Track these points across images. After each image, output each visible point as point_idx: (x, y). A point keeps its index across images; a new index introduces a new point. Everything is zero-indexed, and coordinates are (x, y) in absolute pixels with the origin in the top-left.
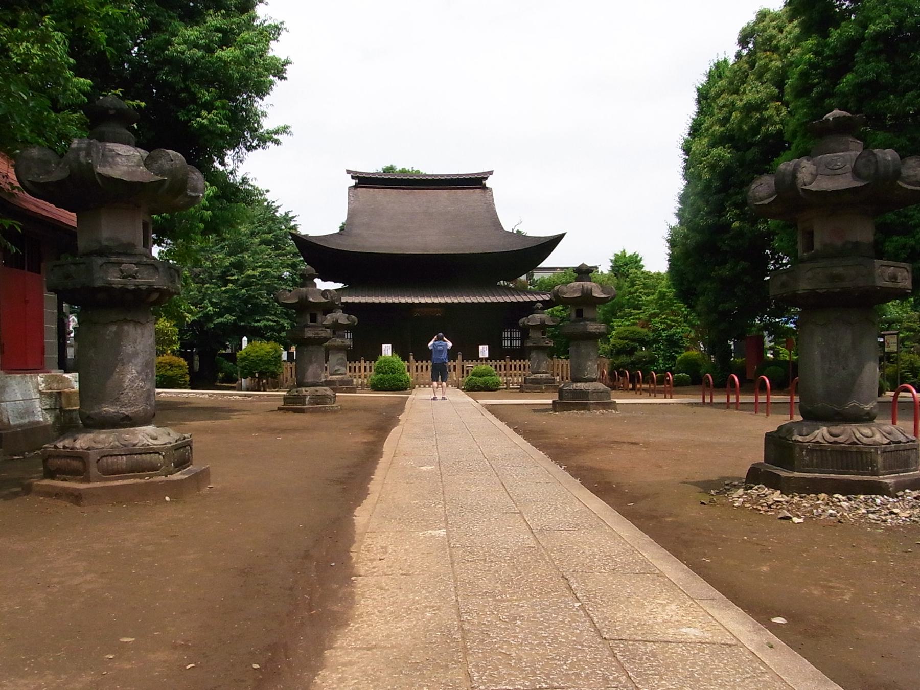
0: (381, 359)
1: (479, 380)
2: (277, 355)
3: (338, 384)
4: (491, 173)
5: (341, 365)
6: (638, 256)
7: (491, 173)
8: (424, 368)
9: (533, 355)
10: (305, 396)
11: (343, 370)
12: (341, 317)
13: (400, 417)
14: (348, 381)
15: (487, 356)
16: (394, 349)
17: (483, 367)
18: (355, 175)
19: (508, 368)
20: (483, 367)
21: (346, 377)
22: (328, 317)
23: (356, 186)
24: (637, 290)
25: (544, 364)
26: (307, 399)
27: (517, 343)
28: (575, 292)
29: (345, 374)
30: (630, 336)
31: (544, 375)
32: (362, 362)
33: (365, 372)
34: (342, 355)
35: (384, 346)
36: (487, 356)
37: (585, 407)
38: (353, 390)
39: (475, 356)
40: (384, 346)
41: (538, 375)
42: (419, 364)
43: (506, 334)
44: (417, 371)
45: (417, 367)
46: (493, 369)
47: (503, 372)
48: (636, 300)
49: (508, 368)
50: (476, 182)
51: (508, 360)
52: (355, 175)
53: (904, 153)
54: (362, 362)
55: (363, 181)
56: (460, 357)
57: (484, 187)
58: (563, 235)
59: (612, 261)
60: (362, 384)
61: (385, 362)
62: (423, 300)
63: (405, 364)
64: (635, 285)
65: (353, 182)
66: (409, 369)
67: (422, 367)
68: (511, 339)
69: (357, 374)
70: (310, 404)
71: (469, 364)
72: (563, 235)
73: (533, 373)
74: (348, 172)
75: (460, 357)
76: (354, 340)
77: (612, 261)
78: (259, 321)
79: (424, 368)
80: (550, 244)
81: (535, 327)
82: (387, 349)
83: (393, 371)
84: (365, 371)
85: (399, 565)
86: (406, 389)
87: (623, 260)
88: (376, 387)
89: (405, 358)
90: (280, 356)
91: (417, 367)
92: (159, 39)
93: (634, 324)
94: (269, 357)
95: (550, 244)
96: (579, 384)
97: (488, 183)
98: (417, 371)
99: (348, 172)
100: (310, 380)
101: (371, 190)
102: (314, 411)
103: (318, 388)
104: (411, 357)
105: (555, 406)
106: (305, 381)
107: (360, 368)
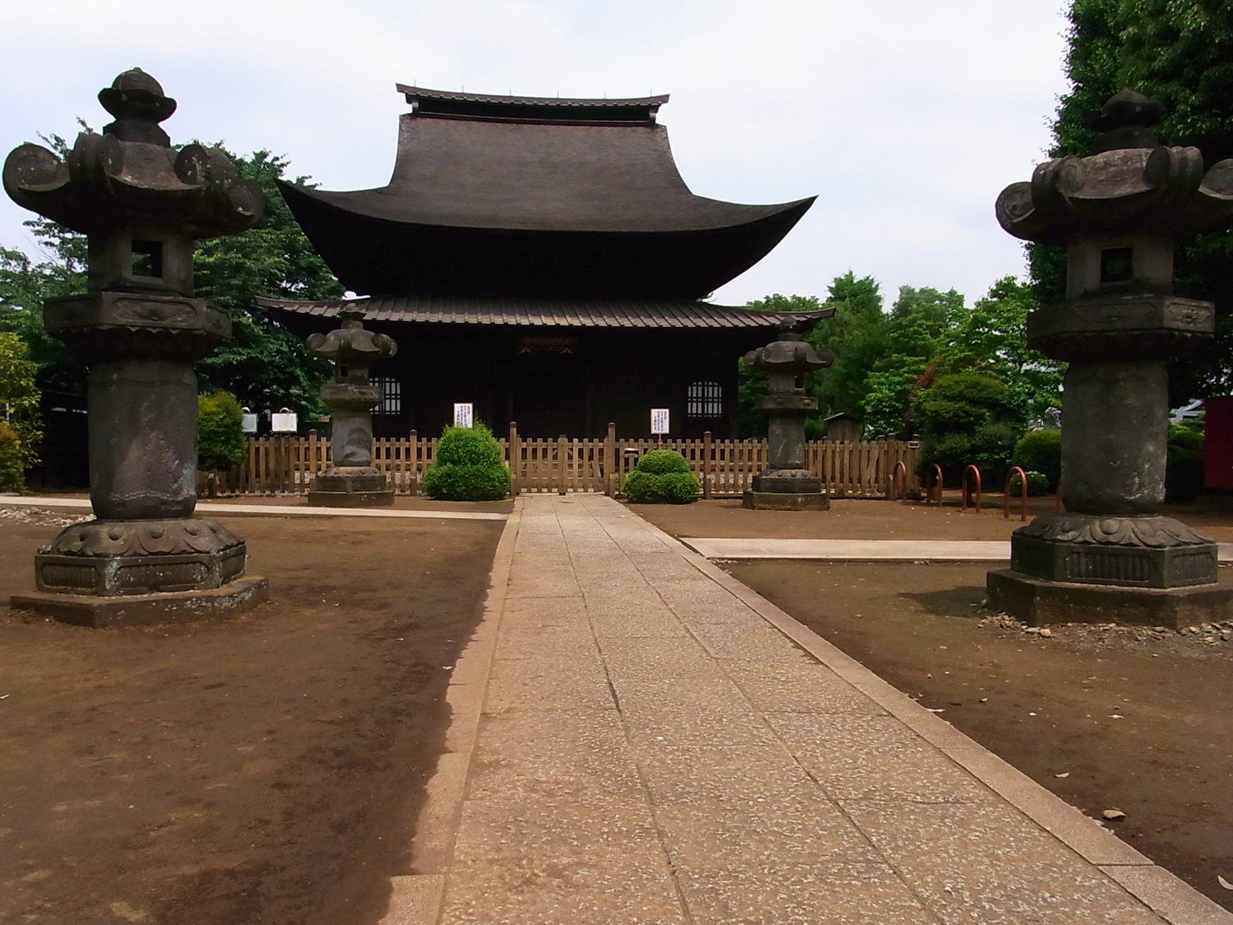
0: (449, 432)
1: (657, 480)
2: (228, 421)
3: (349, 484)
4: (665, 99)
5: (357, 443)
6: (872, 281)
7: (665, 99)
8: (540, 453)
9: (776, 428)
10: (102, 559)
11: (362, 455)
12: (363, 341)
13: (486, 604)
14: (373, 479)
15: (666, 430)
16: (478, 414)
17: (664, 453)
18: (412, 95)
19: (708, 454)
20: (664, 453)
21: (369, 471)
22: (331, 336)
23: (414, 115)
24: (914, 321)
25: (798, 450)
26: (112, 568)
27: (714, 409)
28: (1117, 179)
29: (368, 464)
30: (972, 393)
31: (799, 473)
32: (413, 439)
33: (414, 461)
34: (361, 423)
35: (457, 406)
36: (666, 430)
37: (1155, 611)
38: (383, 500)
39: (641, 430)
40: (457, 406)
41: (787, 473)
42: (529, 444)
43: (694, 391)
44: (524, 457)
45: (524, 450)
46: (679, 454)
47: (698, 462)
48: (911, 338)
49: (708, 454)
50: (638, 114)
51: (708, 440)
52: (412, 95)
53: (1212, 155)
54: (413, 439)
55: (428, 106)
56: (612, 431)
57: (652, 124)
58: (802, 207)
59: (831, 289)
60: (413, 485)
61: (458, 437)
62: (537, 321)
63: (501, 445)
64: (910, 313)
65: (408, 109)
66: (507, 455)
67: (535, 451)
68: (704, 400)
69: (402, 461)
70: (127, 587)
71: (629, 447)
72: (815, 198)
73: (773, 467)
74: (401, 88)
75: (612, 431)
76: (404, 397)
77: (831, 289)
78: (216, 355)
79: (540, 453)
80: (764, 229)
81: (782, 369)
82: (463, 413)
83: (475, 457)
84: (388, 457)
85: (504, 698)
86: (501, 497)
87: (850, 288)
88: (440, 492)
89: (501, 432)
90: (238, 424)
91: (524, 450)
92: (578, 522)
93: (909, 381)
94: (212, 426)
95: (764, 229)
96: (1113, 524)
97: (661, 117)
98: (524, 457)
99: (401, 88)
100: (132, 493)
101: (443, 122)
102: (137, 617)
103: (157, 526)
104: (514, 431)
105: (1007, 592)
106: (115, 497)
107: (408, 450)
